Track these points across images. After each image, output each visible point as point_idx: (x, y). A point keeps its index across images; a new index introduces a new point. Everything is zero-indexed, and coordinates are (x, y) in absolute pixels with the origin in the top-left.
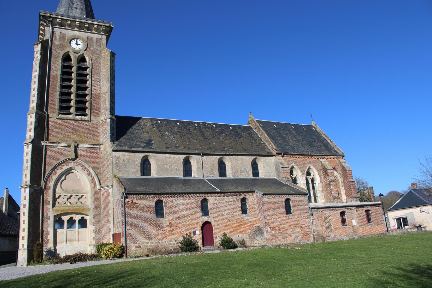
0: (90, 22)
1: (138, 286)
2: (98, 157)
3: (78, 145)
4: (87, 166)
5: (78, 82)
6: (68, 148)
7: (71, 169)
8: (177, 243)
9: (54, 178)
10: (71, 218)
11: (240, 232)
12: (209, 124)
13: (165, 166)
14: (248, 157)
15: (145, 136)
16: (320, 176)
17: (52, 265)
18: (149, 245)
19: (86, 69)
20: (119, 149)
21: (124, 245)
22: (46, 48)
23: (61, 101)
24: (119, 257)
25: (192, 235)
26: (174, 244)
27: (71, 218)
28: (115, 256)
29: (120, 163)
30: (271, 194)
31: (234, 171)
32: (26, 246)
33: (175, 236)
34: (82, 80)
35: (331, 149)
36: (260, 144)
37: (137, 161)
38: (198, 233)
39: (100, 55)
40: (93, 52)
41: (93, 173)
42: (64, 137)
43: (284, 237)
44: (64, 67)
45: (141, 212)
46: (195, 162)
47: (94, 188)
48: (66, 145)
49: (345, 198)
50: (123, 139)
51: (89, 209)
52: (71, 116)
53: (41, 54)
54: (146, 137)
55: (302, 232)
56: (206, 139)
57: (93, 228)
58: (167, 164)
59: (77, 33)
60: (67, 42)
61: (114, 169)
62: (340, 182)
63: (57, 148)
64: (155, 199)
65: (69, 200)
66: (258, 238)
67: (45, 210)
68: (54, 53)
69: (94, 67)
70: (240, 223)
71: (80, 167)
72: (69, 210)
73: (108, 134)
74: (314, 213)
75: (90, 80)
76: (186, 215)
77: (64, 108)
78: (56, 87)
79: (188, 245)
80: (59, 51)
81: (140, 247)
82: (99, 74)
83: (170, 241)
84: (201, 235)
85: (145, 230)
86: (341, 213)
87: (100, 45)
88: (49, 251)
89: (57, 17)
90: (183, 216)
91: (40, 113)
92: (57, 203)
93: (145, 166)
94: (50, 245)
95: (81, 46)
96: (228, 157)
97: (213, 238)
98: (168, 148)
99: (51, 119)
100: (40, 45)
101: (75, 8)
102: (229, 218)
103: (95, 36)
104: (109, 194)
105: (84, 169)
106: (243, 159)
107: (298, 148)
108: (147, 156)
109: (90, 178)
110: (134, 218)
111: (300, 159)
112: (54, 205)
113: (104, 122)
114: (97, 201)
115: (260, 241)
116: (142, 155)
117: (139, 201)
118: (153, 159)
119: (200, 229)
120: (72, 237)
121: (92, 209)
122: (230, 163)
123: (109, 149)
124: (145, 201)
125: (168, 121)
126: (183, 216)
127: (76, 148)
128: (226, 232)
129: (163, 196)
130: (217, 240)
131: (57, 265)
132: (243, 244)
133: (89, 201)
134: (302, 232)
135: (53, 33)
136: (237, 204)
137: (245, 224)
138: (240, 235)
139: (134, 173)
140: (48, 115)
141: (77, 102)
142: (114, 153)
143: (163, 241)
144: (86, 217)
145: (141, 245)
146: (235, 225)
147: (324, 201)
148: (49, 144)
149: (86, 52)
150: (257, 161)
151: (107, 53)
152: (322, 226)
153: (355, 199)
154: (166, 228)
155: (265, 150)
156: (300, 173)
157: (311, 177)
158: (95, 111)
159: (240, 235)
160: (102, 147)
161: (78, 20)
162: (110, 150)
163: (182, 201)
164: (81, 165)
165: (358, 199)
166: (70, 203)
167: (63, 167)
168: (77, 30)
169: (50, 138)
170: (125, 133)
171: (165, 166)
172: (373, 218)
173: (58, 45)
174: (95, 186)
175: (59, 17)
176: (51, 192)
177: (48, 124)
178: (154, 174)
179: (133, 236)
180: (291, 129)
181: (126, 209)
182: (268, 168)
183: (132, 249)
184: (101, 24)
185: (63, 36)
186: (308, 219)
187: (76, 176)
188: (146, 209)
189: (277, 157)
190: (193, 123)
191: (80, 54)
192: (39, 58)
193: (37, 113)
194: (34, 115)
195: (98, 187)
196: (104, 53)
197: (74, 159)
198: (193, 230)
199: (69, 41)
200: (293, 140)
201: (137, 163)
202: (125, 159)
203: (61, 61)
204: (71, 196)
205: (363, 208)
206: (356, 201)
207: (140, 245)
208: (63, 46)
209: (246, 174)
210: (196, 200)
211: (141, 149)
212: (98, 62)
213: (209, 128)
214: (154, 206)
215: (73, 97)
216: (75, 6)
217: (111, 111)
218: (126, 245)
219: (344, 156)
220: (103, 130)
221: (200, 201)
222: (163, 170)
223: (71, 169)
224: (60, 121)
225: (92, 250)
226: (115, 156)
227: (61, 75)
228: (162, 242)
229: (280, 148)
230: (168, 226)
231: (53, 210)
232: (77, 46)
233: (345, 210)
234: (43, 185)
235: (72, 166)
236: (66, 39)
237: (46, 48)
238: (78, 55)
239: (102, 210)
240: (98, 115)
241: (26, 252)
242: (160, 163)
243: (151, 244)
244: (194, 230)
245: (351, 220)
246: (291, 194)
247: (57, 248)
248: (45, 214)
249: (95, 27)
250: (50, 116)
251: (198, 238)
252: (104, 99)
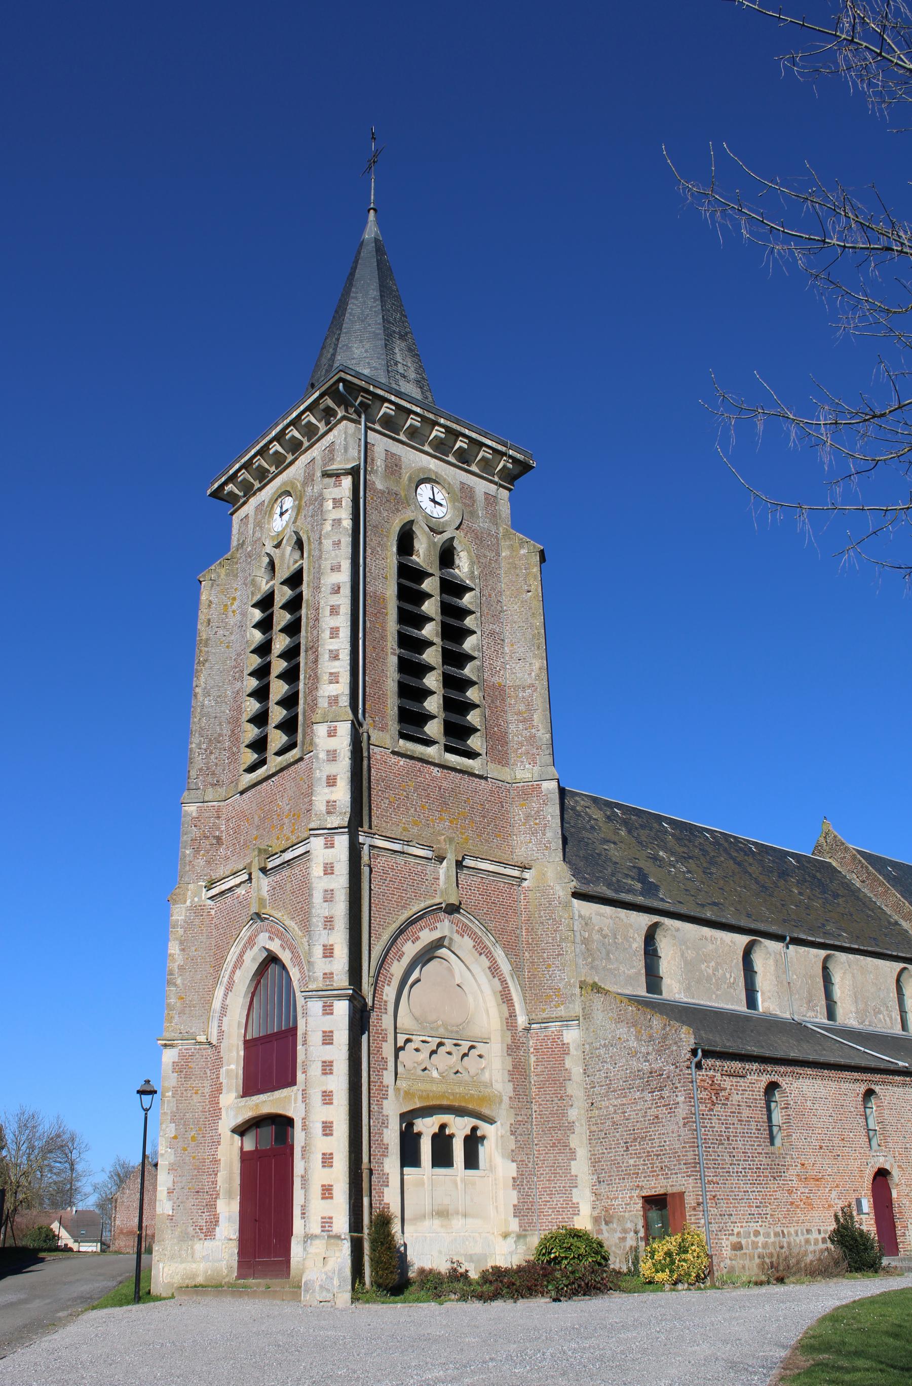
6: (430, 867)
7: (438, 944)
13: (703, 967)
18: (761, 1239)
29: (593, 941)
36: (889, 922)
37: (634, 940)
41: (505, 967)
42: (415, 824)
45: (735, 1120)
46: (771, 962)
48: (428, 854)
52: (432, 752)
57: (511, 1170)
59: (433, 464)
60: (409, 486)
63: (400, 859)
71: (467, 942)
72: (443, 1096)
73: (549, 834)
77: (411, 721)
78: (383, 638)
80: (385, 514)
81: (741, 1248)
87: (494, 517)
89: (387, 395)
95: (444, 510)
97: (895, 1227)
99: (377, 750)
103: (481, 487)
104: (564, 1049)
105: (482, 949)
113: (530, 791)
114: (518, 1072)
117: (728, 1083)
121: (506, 1099)
122: (849, 976)
123: (558, 887)
129: (782, 1069)
131: (498, 1304)
133: (493, 1070)
143: (792, 1230)
145: (743, 1242)
151: (523, 551)
154: (795, 1183)
160: (526, 875)
161: (442, 421)
163: (823, 1092)
167: (421, 934)
168: (431, 451)
173: (383, 492)
174: (512, 1015)
175: (393, 398)
184: (503, 449)
185: (394, 466)
187: (450, 970)
196: (511, 547)
199: (414, 485)
201: (635, 945)
202: (606, 931)
203: (395, 549)
220: (528, 817)
224: (402, 761)
225: (511, 1253)
235: (446, 933)
236: (405, 477)
239: (535, 1108)
242: (690, 954)
248: (374, 1107)
252: (522, 707)
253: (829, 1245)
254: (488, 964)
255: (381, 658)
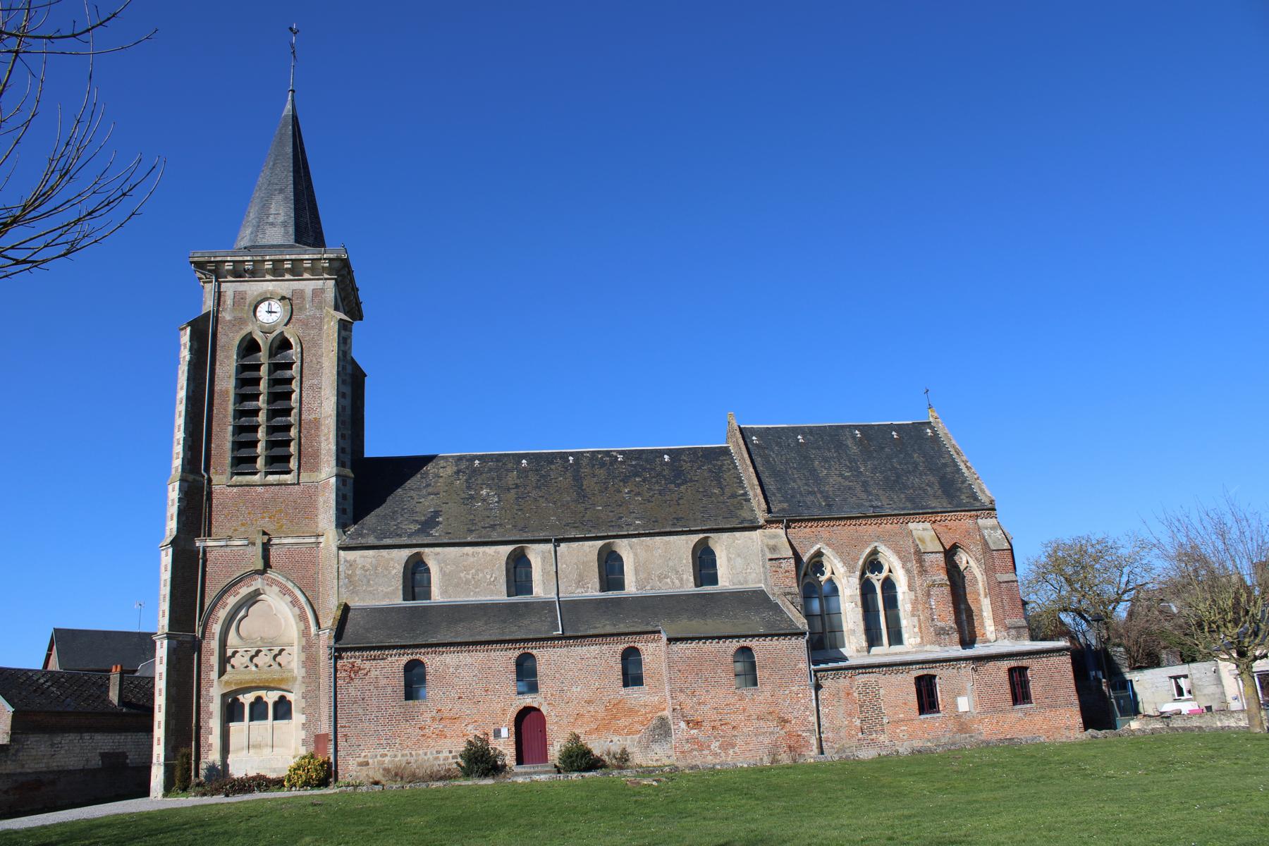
0: (293, 257)
1: (762, 841)
2: (314, 564)
3: (270, 540)
4: (290, 585)
5: (273, 397)
6: (250, 549)
7: (257, 593)
8: (454, 757)
9: (222, 614)
10: (259, 699)
11: (616, 732)
12: (608, 453)
14: (683, 537)
15: (427, 504)
16: (908, 571)
17: (198, 798)
18: (387, 759)
19: (289, 366)
20: (353, 543)
21: (332, 760)
22: (204, 334)
23: (237, 445)
24: (318, 786)
25: (492, 738)
26: (446, 759)
27: (259, 699)
28: (306, 784)
30: (693, 639)
31: (642, 576)
32: (162, 759)
33: (448, 741)
34: (281, 394)
35: (960, 490)
38: (504, 732)
39: (321, 329)
40: (305, 324)
42: (243, 525)
43: (726, 746)
44: (242, 368)
45: (372, 688)
47: (305, 633)
48: (246, 542)
49: (992, 628)
50: (371, 519)
51: (295, 679)
52: (256, 478)
53: (191, 350)
54: (429, 507)
55: (782, 732)
56: (582, 495)
57: (303, 719)
58: (466, 569)
61: (343, 590)
62: (980, 584)
63: (228, 550)
64: (405, 659)
65: (255, 660)
66: (656, 747)
67: (203, 683)
68: (222, 339)
69: (307, 359)
70: (616, 711)
71: (276, 589)
74: (826, 683)
75: (298, 390)
76: (478, 692)
77: (243, 463)
78: (225, 416)
79: (480, 761)
81: (367, 764)
82: (317, 373)
83: (438, 752)
84: (513, 738)
85: (380, 728)
86: (1011, 670)
88: (212, 768)
90: (471, 696)
91: (191, 477)
92: (229, 668)
93: (418, 576)
94: (212, 756)
96: (625, 541)
98: (471, 531)
100: (189, 329)
101: (272, 224)
102: (586, 697)
103: (308, 286)
105: (285, 591)
106: (668, 543)
107: (845, 500)
108: (418, 554)
109: (297, 610)
110: (356, 702)
111: (844, 531)
112: (222, 672)
115: (661, 755)
116: (406, 553)
117: (367, 665)
118: (435, 560)
119: (512, 724)
120: (259, 739)
121: (300, 679)
122: (631, 555)
124: (381, 662)
125: (499, 458)
126: (471, 696)
127: (266, 548)
128: (577, 731)
130: (555, 751)
132: (623, 759)
134: (782, 732)
135: (219, 295)
136: (612, 664)
137: (631, 712)
138: (615, 739)
139: (386, 595)
140: (210, 480)
141: (271, 445)
142: (341, 552)
144: (290, 697)
145: (370, 761)
146: (602, 713)
147: (919, 640)
148: (210, 543)
149: (290, 326)
150: (711, 543)
152: (850, 715)
153: (1013, 632)
154: (429, 722)
155: (739, 512)
156: (840, 569)
157: (885, 574)
158: (309, 460)
159: (615, 739)
160: (321, 539)
162: (334, 549)
163: (469, 660)
164: (278, 584)
165: (1026, 633)
166: (257, 666)
169: (214, 530)
170: (380, 502)
171: (466, 574)
172: (1035, 688)
174: (307, 627)
176: (215, 644)
177: (210, 498)
178: (438, 595)
179: (353, 741)
180: (849, 442)
181: (340, 682)
182: (745, 560)
183: (350, 768)
185: (239, 298)
186: (804, 698)
188: (383, 682)
189: (768, 531)
190: (564, 456)
191: (275, 333)
192: (188, 358)
193: (182, 480)
194: (177, 484)
195: (313, 629)
197: (262, 572)
198: (493, 727)
200: (841, 475)
204: (258, 652)
205: (999, 663)
206: (1018, 637)
207: (364, 761)
208: (241, 322)
209: (677, 582)
210: (505, 659)
211: (405, 540)
212: (316, 344)
213: (603, 464)
214: (402, 674)
215: (261, 434)
216: (271, 219)
217: (337, 459)
218: (336, 761)
219: (994, 509)
221: (513, 661)
222: (457, 585)
223: (257, 593)
224: (235, 489)
226: (346, 561)
227: (236, 388)
228: (418, 755)
229: (785, 505)
230: (433, 719)
231: (220, 682)
232: (270, 315)
233: (932, 672)
234: (199, 634)
235: (259, 586)
237: (204, 334)
238: (271, 337)
240: (315, 468)
241: (162, 769)
242: (448, 569)
243: (392, 757)
244: (496, 727)
245: (956, 697)
246: (753, 636)
247: (229, 761)
248: (203, 692)
249: (307, 265)
250: (214, 482)
251: (504, 746)
253: (459, 760)
254: (290, 599)
255: (223, 430)
